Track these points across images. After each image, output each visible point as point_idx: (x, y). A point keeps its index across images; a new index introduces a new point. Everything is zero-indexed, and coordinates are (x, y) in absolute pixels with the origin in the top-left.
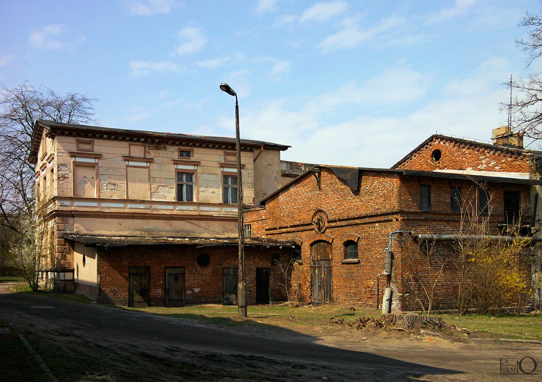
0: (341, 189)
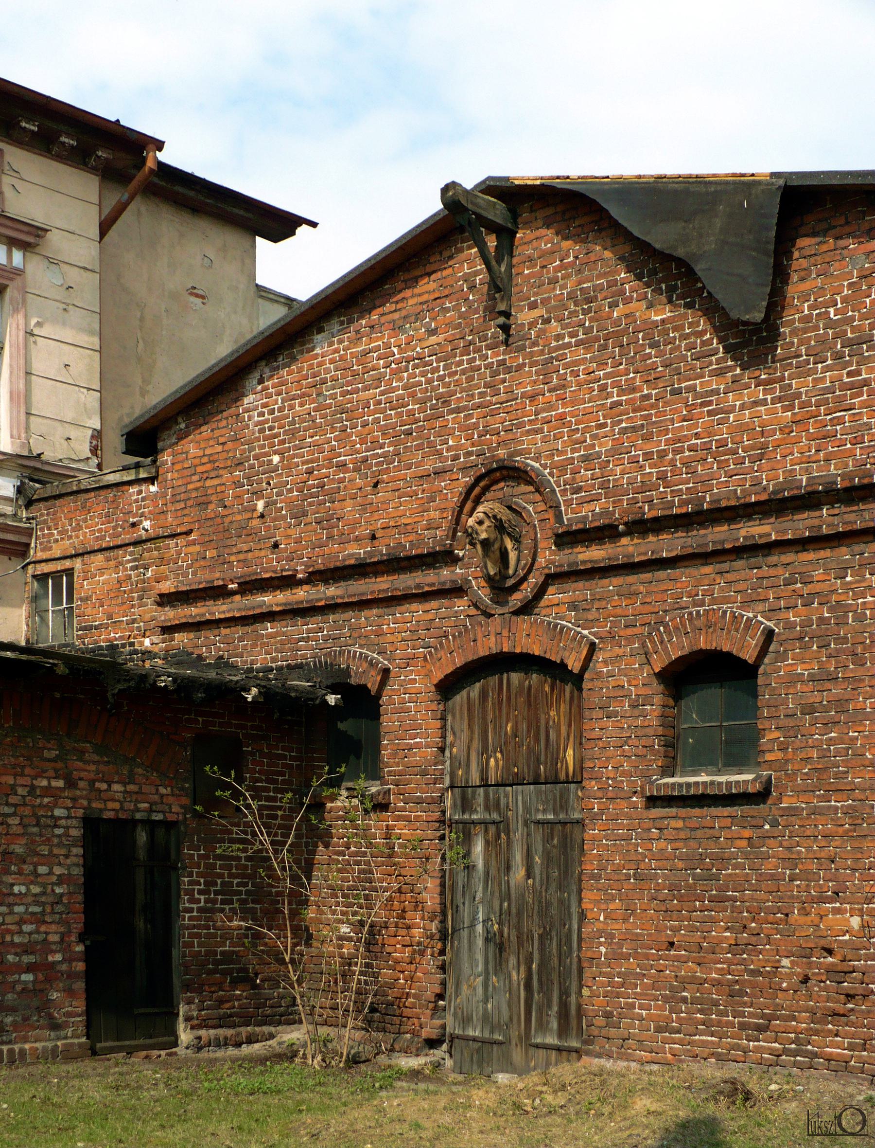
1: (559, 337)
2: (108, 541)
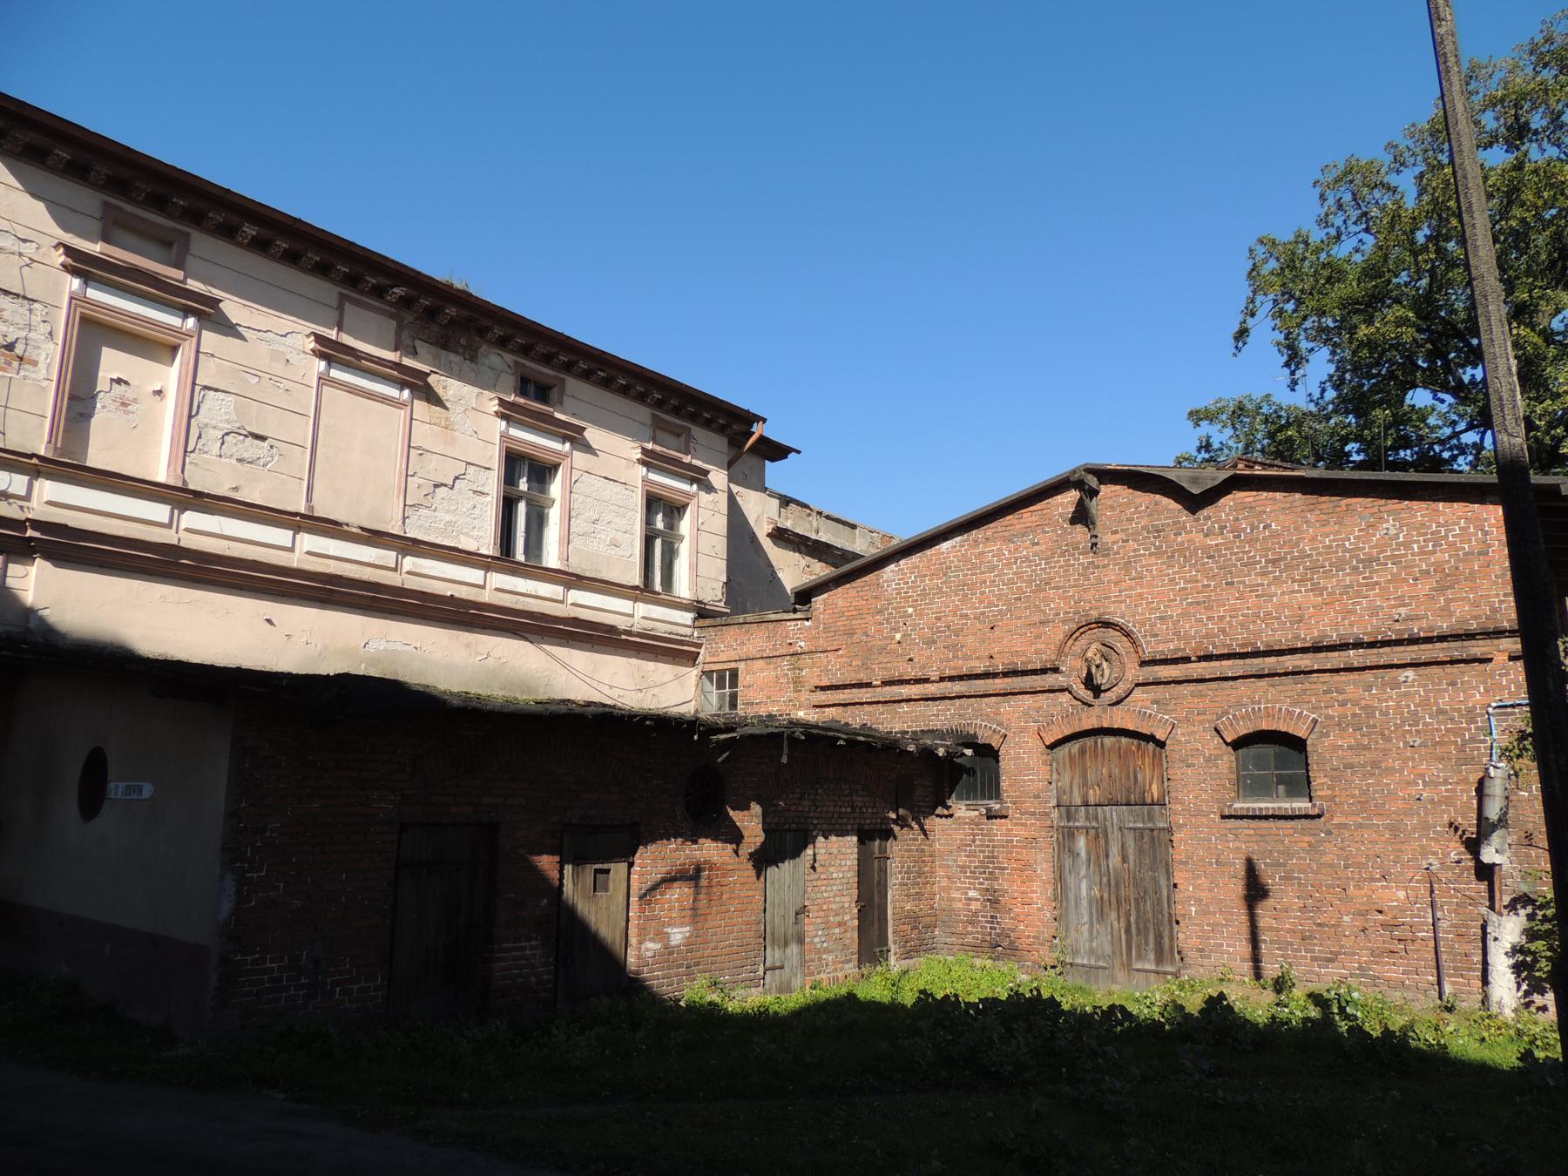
0: (1206, 549)
1: (1135, 550)
2: (768, 653)
